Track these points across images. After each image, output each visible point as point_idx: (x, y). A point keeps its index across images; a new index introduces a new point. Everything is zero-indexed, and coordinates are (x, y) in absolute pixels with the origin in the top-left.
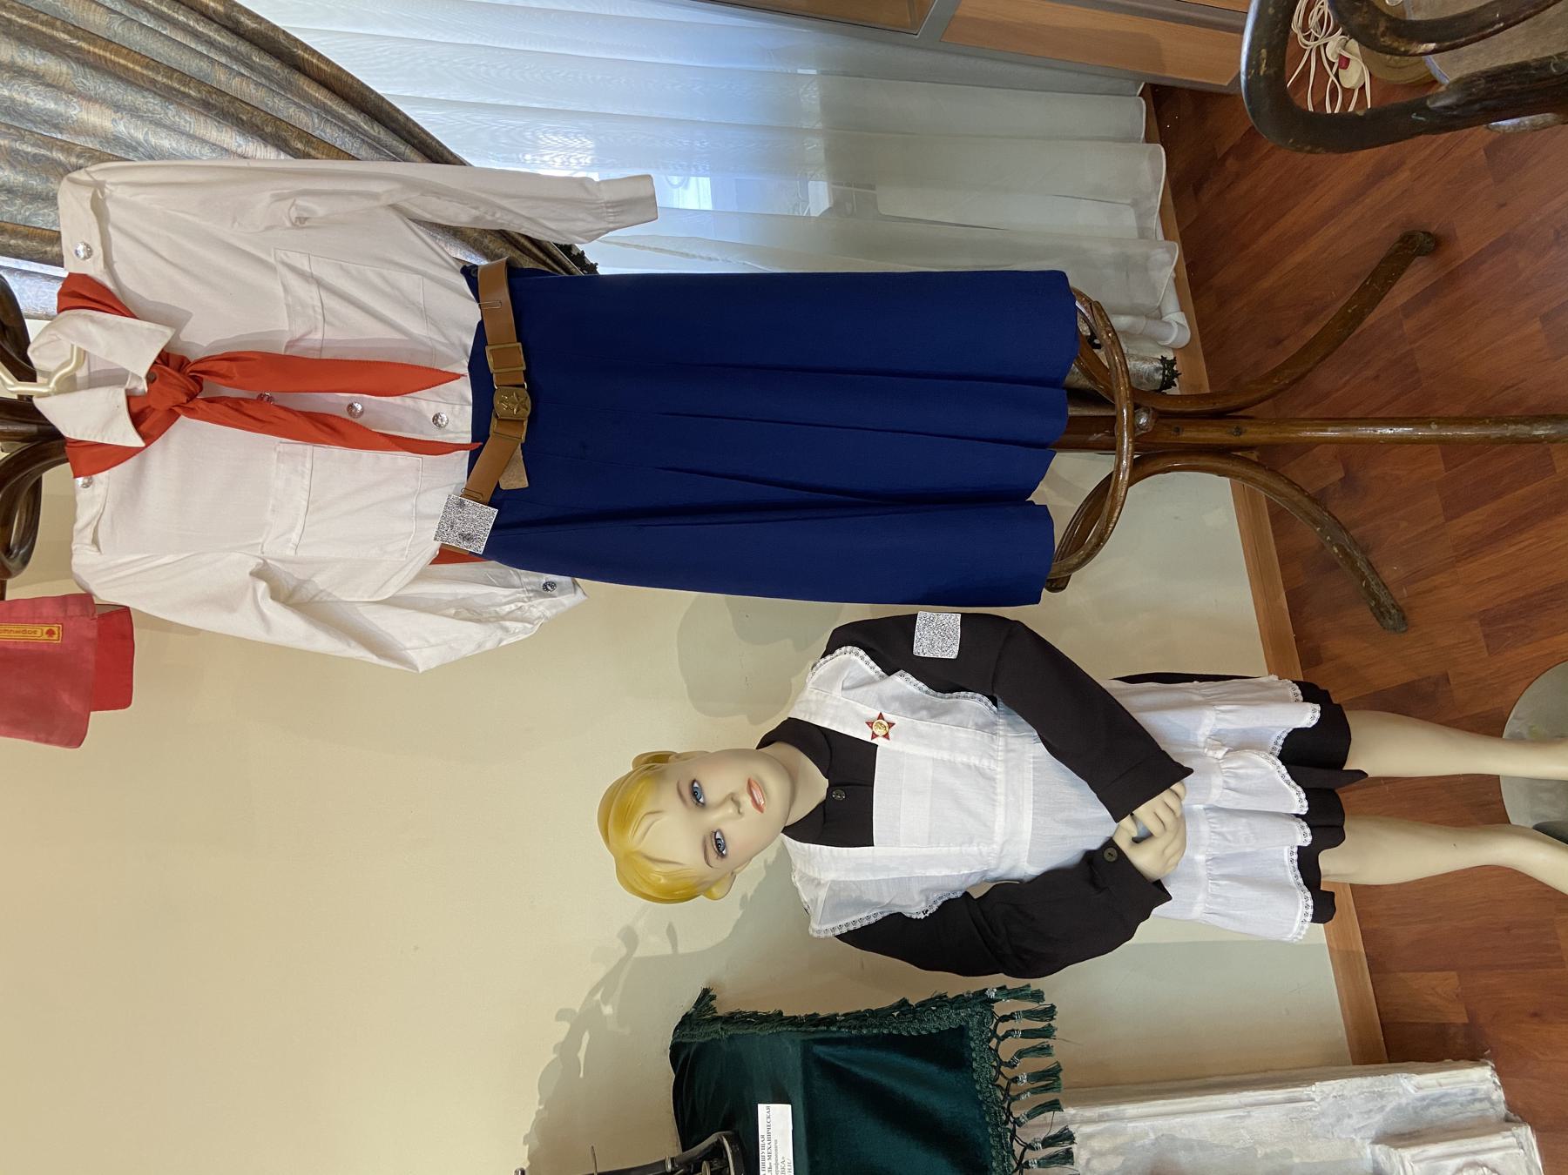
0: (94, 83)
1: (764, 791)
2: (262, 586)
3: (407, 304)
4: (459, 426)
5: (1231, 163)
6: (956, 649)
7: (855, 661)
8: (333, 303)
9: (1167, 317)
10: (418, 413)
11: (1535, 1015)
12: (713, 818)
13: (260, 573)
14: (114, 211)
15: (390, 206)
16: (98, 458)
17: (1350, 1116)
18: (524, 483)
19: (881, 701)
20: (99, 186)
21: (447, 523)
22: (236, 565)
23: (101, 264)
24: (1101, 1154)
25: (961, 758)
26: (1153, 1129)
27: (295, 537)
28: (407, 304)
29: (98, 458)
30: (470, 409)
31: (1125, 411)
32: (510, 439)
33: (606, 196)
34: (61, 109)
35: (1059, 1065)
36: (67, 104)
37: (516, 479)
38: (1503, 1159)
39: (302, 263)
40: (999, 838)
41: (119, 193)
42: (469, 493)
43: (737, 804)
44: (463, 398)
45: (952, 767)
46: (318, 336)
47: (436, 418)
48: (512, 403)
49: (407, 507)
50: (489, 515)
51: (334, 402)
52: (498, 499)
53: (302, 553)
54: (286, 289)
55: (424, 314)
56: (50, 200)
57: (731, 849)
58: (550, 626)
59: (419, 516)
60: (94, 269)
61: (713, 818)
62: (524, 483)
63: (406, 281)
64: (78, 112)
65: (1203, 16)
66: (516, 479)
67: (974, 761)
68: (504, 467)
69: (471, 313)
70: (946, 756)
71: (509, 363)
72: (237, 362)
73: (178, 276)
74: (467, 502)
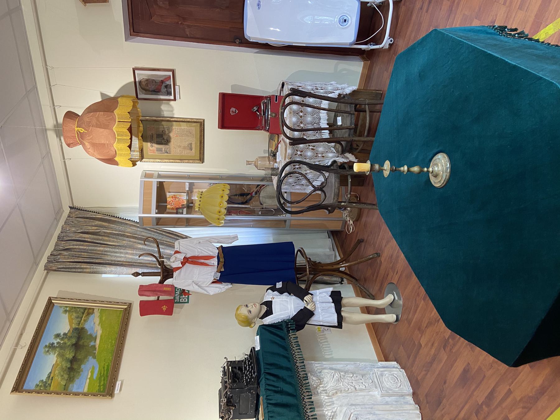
0: (167, 248)
1: (256, 305)
3: (210, 251)
4: (216, 264)
5: (345, 241)
7: (270, 291)
8: (202, 251)
10: (211, 263)
11: (399, 348)
12: (249, 308)
14: (180, 244)
17: (367, 368)
18: (224, 270)
19: (273, 295)
21: (214, 275)
22: (190, 281)
23: (179, 249)
24: (319, 369)
25: (283, 300)
26: (329, 367)
27: (197, 278)
28: (210, 251)
30: (217, 262)
32: (222, 264)
33: (232, 237)
34: (164, 251)
36: (165, 250)
37: (223, 270)
38: (397, 373)
39: (199, 247)
40: (289, 309)
41: (181, 242)
43: (252, 306)
44: (216, 261)
45: (282, 301)
46: (200, 255)
47: (213, 263)
48: (222, 260)
49: (210, 274)
52: (221, 272)
53: (198, 280)
54: (197, 250)
55: (212, 252)
57: (252, 312)
58: (227, 290)
59: (211, 275)
60: (178, 250)
61: (249, 308)
62: (224, 270)
63: (210, 249)
66: (223, 270)
67: (285, 300)
69: (217, 251)
70: (281, 299)
71: (222, 256)
73: (186, 250)
74: (217, 273)
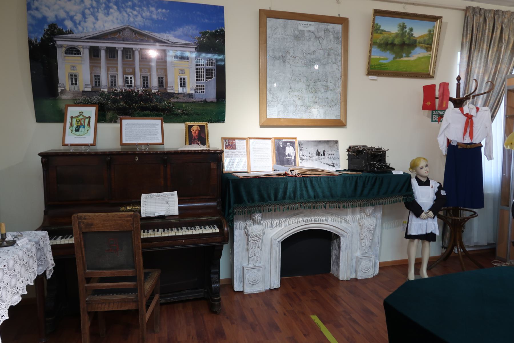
1: (427, 173)
2: (449, 124)
4: (465, 142)
6: (442, 194)
7: (438, 185)
9: (493, 184)
13: (450, 124)
15: (488, 134)
16: (462, 111)
19: (435, 187)
20: (488, 110)
21: (454, 141)
29: (462, 111)
31: (459, 248)
35: (215, 313)
37: (459, 147)
42: (458, 143)
50: (456, 145)
51: (468, 130)
52: (457, 145)
56: (488, 106)
57: (421, 170)
60: (480, 110)
64: (485, 45)
65: (474, 39)
66: (459, 147)
68: (461, 146)
72: (472, 123)
74: (457, 143)
